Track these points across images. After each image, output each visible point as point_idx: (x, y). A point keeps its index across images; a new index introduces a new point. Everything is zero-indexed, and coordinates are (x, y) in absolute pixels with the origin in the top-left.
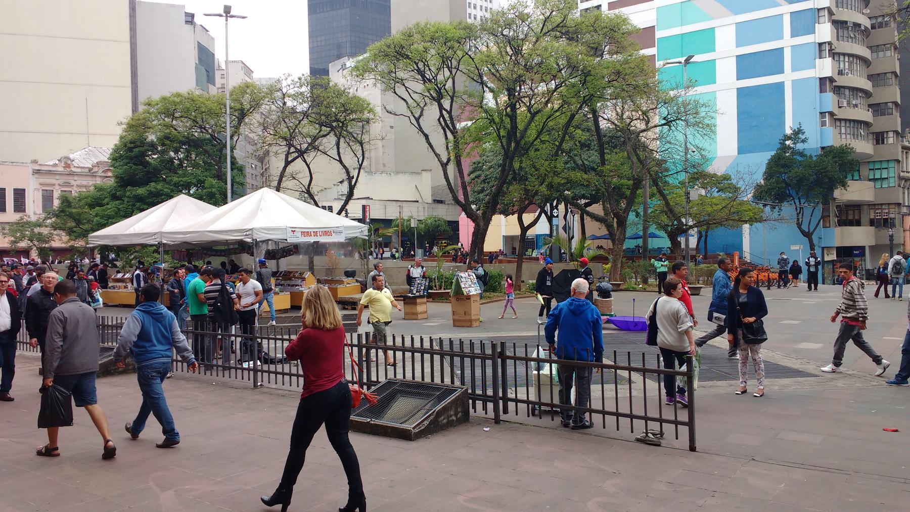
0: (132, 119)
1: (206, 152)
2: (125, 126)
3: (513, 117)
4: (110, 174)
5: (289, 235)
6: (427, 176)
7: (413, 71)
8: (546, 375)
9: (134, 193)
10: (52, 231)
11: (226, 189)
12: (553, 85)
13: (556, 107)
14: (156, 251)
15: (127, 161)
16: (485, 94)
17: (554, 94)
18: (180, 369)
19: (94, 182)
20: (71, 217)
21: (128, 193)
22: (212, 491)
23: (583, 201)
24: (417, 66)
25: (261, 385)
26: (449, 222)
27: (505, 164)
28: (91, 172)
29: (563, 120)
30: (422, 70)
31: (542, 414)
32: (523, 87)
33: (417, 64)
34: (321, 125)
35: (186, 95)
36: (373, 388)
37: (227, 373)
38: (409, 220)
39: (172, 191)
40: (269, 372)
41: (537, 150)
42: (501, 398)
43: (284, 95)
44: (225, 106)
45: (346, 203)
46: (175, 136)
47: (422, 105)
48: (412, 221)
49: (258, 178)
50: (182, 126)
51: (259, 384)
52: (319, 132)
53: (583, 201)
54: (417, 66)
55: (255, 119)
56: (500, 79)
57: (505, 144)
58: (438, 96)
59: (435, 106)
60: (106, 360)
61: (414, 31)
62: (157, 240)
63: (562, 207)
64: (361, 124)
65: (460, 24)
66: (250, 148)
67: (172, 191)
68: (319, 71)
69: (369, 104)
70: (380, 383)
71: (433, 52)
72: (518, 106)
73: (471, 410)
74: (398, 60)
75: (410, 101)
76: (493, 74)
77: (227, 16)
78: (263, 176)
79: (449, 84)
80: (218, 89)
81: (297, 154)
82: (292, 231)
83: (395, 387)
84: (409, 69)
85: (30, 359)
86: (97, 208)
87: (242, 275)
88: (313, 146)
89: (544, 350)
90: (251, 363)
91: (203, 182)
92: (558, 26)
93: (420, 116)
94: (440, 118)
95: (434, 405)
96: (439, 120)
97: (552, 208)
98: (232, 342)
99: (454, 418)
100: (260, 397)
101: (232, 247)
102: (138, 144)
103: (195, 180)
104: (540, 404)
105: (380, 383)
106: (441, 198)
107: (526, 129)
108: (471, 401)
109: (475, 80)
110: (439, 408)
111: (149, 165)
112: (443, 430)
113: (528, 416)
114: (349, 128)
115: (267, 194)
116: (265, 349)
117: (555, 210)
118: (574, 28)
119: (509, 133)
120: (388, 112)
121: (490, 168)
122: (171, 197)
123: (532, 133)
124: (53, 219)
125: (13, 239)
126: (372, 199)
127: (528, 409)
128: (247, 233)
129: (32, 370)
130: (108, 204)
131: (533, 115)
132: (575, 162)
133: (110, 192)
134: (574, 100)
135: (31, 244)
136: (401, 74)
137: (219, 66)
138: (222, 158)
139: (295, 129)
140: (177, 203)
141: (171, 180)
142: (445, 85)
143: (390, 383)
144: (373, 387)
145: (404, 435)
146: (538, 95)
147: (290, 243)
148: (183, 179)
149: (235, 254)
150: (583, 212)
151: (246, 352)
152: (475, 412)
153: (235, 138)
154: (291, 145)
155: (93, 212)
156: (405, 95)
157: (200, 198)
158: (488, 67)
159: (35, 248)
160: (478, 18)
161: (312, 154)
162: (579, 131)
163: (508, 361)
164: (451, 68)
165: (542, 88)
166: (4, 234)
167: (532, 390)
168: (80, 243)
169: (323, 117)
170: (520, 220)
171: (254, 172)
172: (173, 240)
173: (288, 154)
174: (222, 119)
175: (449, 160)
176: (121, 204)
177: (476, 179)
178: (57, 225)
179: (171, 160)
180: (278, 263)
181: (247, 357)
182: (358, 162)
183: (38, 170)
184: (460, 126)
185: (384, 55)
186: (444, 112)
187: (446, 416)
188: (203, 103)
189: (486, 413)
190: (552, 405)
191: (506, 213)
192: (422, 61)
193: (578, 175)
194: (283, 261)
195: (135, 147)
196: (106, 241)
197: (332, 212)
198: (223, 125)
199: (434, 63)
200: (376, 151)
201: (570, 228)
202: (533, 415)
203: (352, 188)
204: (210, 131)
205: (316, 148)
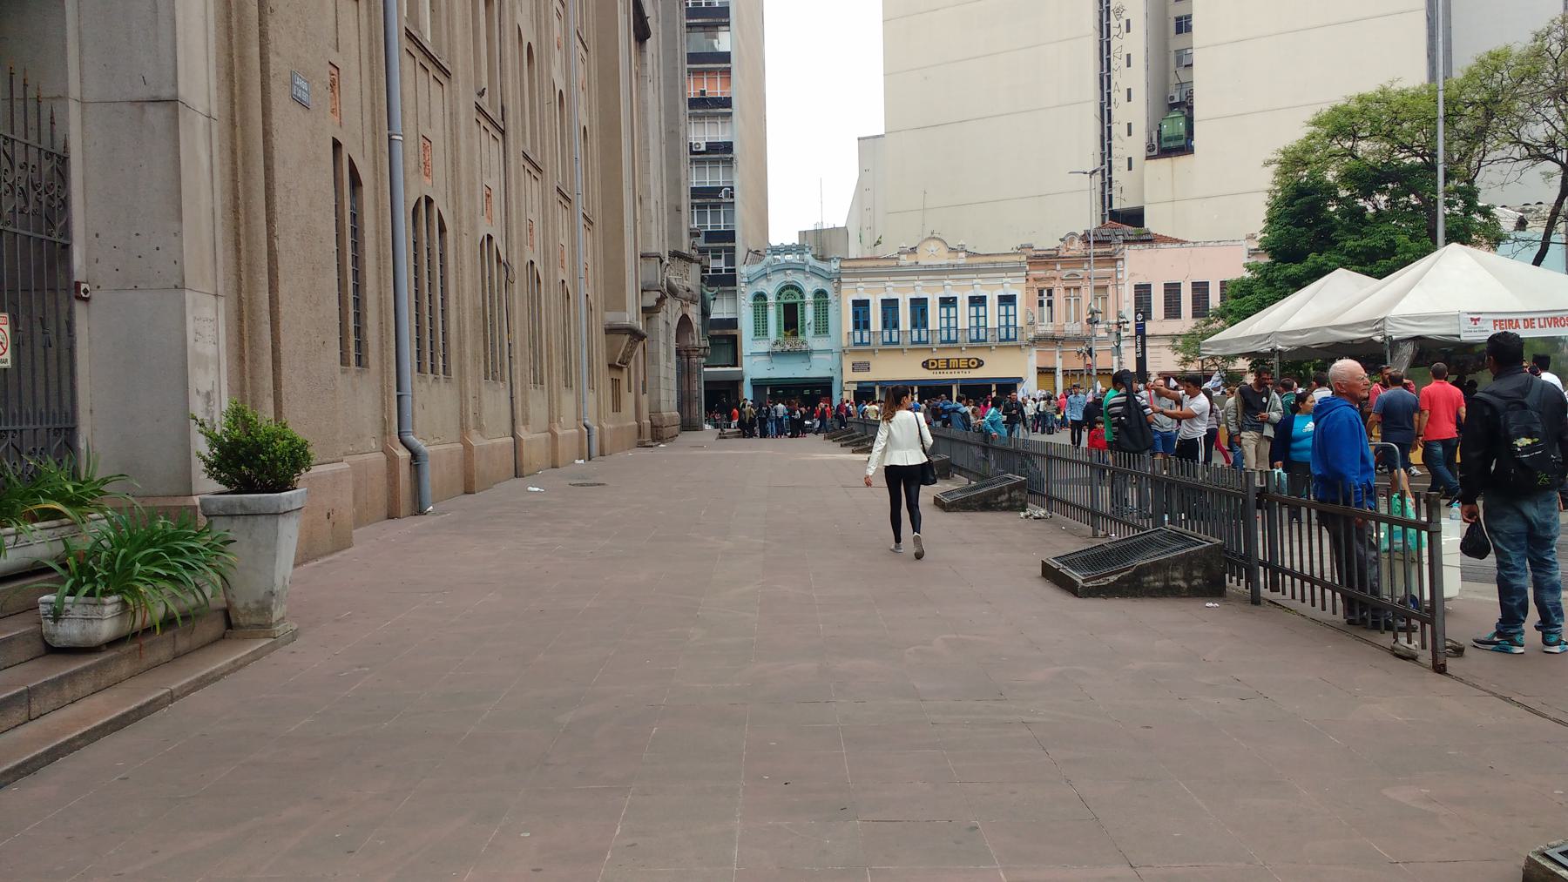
2: (1275, 167)
5: (1464, 327)
62: (1271, 345)
82: (1472, 319)
98: (1165, 469)
128: (1378, 326)
172: (1290, 344)
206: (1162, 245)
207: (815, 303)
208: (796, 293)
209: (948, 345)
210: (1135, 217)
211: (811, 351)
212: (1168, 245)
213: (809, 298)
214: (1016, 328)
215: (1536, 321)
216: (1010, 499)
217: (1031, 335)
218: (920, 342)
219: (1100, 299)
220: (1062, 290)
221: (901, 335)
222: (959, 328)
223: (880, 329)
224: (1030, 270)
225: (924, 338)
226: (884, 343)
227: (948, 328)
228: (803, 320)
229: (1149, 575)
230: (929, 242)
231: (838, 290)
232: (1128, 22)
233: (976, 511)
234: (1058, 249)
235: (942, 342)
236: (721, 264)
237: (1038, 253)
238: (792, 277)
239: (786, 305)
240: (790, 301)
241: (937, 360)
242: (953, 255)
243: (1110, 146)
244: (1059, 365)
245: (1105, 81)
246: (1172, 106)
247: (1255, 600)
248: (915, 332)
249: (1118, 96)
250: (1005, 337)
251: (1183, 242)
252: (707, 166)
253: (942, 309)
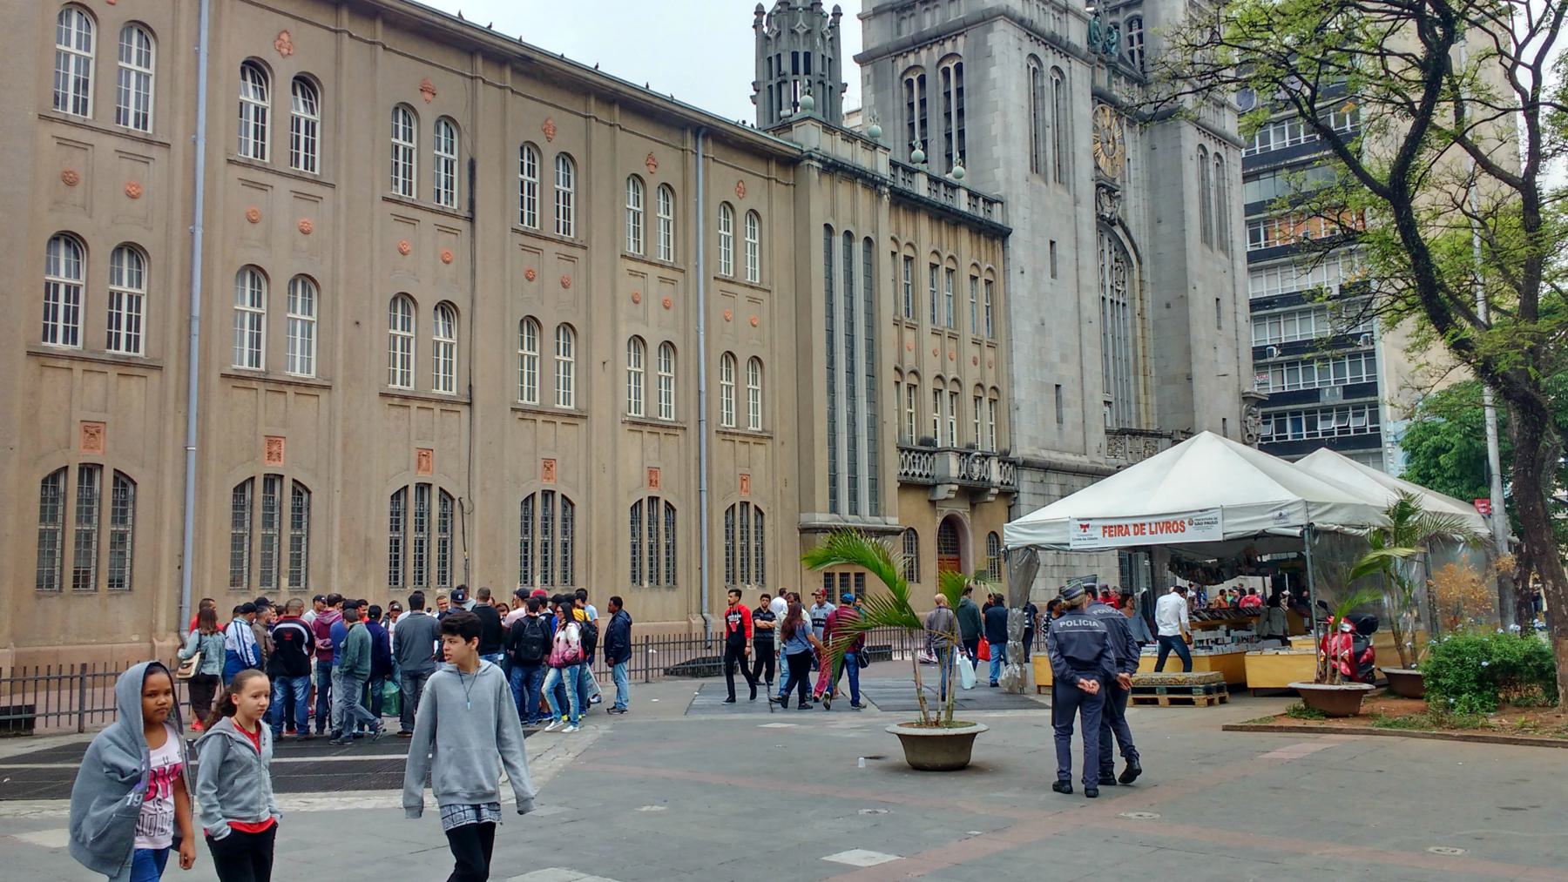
5: (1074, 535)
82: (1082, 526)
215: (1147, 527)
236: (1364, 421)
252: (1297, 318)
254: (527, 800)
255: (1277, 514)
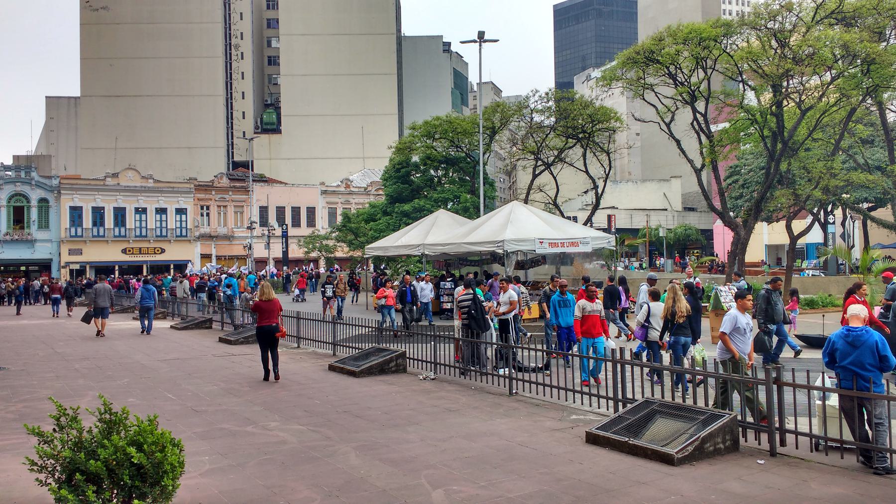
0: (400, 143)
1: (461, 168)
2: (394, 150)
3: (779, 116)
4: (381, 192)
5: (537, 247)
6: (676, 184)
7: (663, 75)
8: (833, 407)
9: (401, 209)
10: (336, 243)
11: (479, 203)
12: (828, 77)
13: (832, 101)
14: (420, 262)
15: (396, 180)
16: (746, 92)
17: (830, 87)
18: (443, 372)
19: (369, 201)
20: (350, 231)
21: (396, 209)
22: (477, 494)
23: (866, 205)
24: (669, 70)
25: (516, 393)
26: (702, 230)
27: (769, 168)
28: (366, 192)
29: (843, 113)
30: (673, 73)
31: (828, 449)
32: (791, 82)
33: (668, 68)
34: (568, 137)
35: (445, 118)
36: (629, 406)
37: (484, 378)
38: (657, 229)
39: (433, 206)
40: (524, 381)
41: (808, 150)
42: (777, 429)
43: (532, 111)
44: (479, 126)
45: (593, 214)
46: (436, 156)
47: (673, 109)
48: (661, 230)
49: (506, 191)
50: (440, 147)
51: (514, 391)
52: (566, 144)
53: (866, 205)
54: (669, 70)
55: (504, 136)
56: (764, 76)
57: (769, 145)
58: (692, 99)
59: (689, 109)
60: (382, 360)
61: (666, 34)
62: (421, 251)
63: (839, 212)
64: (607, 134)
65: (717, 21)
66: (500, 164)
67: (433, 206)
68: (564, 84)
69: (616, 113)
70: (637, 401)
71: (686, 54)
72: (785, 103)
73: (742, 440)
74: (648, 65)
75: (660, 106)
76: (755, 71)
77: (480, 42)
78: (510, 189)
79: (703, 87)
80: (471, 110)
81: (544, 167)
82: (540, 242)
83: (654, 407)
84: (659, 74)
85: (321, 355)
86: (372, 223)
87: (503, 284)
88: (560, 159)
89: (829, 377)
90: (507, 369)
91: (459, 198)
92: (833, 13)
93: (671, 121)
94: (693, 122)
95: (699, 430)
96: (692, 124)
97: (827, 214)
99: (721, 446)
100: (516, 405)
101: (484, 257)
102: (405, 164)
103: (452, 196)
104: (827, 439)
105: (637, 401)
106: (692, 205)
107: (795, 128)
108: (740, 429)
109: (734, 80)
110: (704, 433)
111: (413, 182)
112: (709, 458)
113: (812, 451)
114: (596, 138)
115: (516, 208)
116: (519, 358)
117: (831, 217)
118: (852, 13)
119: (774, 134)
120: (636, 119)
121: (749, 172)
122: (432, 212)
123: (802, 131)
124: (337, 233)
125: (306, 250)
126: (617, 208)
127: (811, 443)
128: (499, 245)
129: (323, 365)
130: (380, 219)
131: (804, 113)
132: (855, 161)
133: (382, 208)
134: (855, 92)
135: (321, 254)
136: (650, 80)
137: (472, 89)
138: (475, 175)
139: (542, 143)
140: (437, 217)
141: (432, 197)
142: (699, 88)
143: (647, 403)
144: (629, 405)
145: (666, 459)
146: (810, 90)
147: (538, 254)
148: (442, 195)
149: (488, 264)
150: (866, 217)
151: (502, 359)
152: (746, 441)
153: (486, 156)
154: (539, 158)
155: (368, 227)
156: (655, 101)
157: (457, 212)
158: (748, 64)
159: (323, 258)
160: (734, 14)
161: (559, 166)
162: (860, 126)
163: (785, 388)
164: (706, 68)
165: (815, 81)
166: (300, 245)
167: (815, 421)
168: (358, 254)
169: (570, 130)
170: (789, 228)
171: (503, 186)
173: (536, 167)
174: (475, 138)
175: (703, 166)
176: (391, 219)
177: (734, 185)
178: (340, 238)
179: (431, 179)
180: (526, 273)
181: (501, 364)
182: (605, 172)
183: (326, 191)
184: (713, 128)
185: (632, 62)
186: (698, 116)
187: (712, 442)
188: (458, 124)
189: (760, 444)
190: (842, 442)
191: (769, 221)
192: (674, 65)
193: (859, 177)
194: (531, 271)
195: (403, 168)
196: (379, 252)
197: (577, 222)
198: (476, 144)
199: (686, 64)
200: (622, 161)
201: (849, 236)
202: (817, 450)
203: (598, 198)
204: (465, 150)
205: (562, 160)
206: (275, 184)
207: (39, 207)
208: (24, 199)
209: (141, 239)
210: (246, 165)
211: (35, 241)
212: (278, 185)
213: (34, 203)
214: (147, 229)
216: (397, 365)
217: (197, 234)
218: (120, 236)
219: (239, 213)
220: (216, 207)
221: (106, 231)
222: (148, 227)
223: (112, 227)
224: (195, 194)
225: (123, 233)
226: (94, 236)
227: (141, 228)
228: (29, 218)
229: (707, 443)
230: (128, 171)
231: (58, 199)
232: (242, 53)
233: (376, 375)
234: (212, 181)
235: (136, 236)
237: (200, 183)
238: (20, 188)
239: (15, 208)
240: (18, 204)
241: (133, 248)
242: (145, 180)
243: (232, 123)
244: (214, 253)
245: (229, 85)
246: (267, 106)
247: (773, 453)
248: (95, 230)
249: (237, 95)
250: (179, 235)
251: (286, 184)
253: (136, 215)
254: (117, 177)
255: (608, 241)
